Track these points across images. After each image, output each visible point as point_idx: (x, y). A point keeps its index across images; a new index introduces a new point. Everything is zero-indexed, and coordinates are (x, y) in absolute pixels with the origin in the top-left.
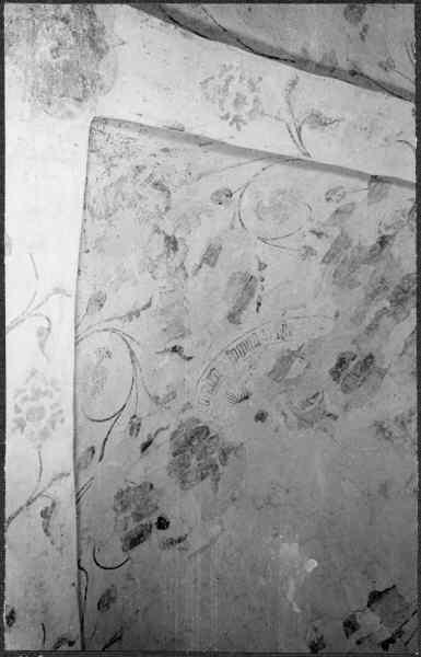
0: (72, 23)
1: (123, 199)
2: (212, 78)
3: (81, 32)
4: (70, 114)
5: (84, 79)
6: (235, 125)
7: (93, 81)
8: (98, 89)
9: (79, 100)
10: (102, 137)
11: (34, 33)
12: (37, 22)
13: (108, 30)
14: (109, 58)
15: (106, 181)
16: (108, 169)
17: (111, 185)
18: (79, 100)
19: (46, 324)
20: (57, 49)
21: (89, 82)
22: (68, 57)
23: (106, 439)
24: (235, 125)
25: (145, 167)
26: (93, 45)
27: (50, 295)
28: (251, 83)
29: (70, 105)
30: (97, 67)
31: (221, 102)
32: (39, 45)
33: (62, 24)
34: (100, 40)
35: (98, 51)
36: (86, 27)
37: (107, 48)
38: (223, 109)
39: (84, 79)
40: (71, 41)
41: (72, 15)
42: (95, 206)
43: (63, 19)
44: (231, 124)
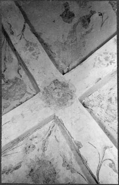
0: (57, 88)
1: (115, 111)
2: (95, 63)
3: (60, 87)
4: (72, 103)
5: (69, 94)
6: (112, 64)
7: (71, 92)
8: (73, 93)
9: (71, 98)
10: (91, 102)
11: (52, 96)
12: (51, 94)
13: (65, 81)
14: (70, 85)
15: (104, 111)
16: (101, 107)
17: (107, 110)
18: (71, 98)
19: (111, 162)
20: (59, 95)
21: (70, 93)
22: (62, 94)
23: (93, 145)
24: (112, 64)
25: (111, 98)
26: (64, 86)
27: (104, 151)
28: (104, 53)
29: (70, 101)
30: (69, 89)
31: (102, 64)
32: (7, 81)
33: (56, 90)
34: (65, 85)
35: (67, 86)
36: (60, 85)
37: (68, 84)
38: (105, 65)
39: (69, 94)
40: (60, 90)
41: (56, 87)
42: (108, 119)
43: (55, 89)
44: (111, 64)
